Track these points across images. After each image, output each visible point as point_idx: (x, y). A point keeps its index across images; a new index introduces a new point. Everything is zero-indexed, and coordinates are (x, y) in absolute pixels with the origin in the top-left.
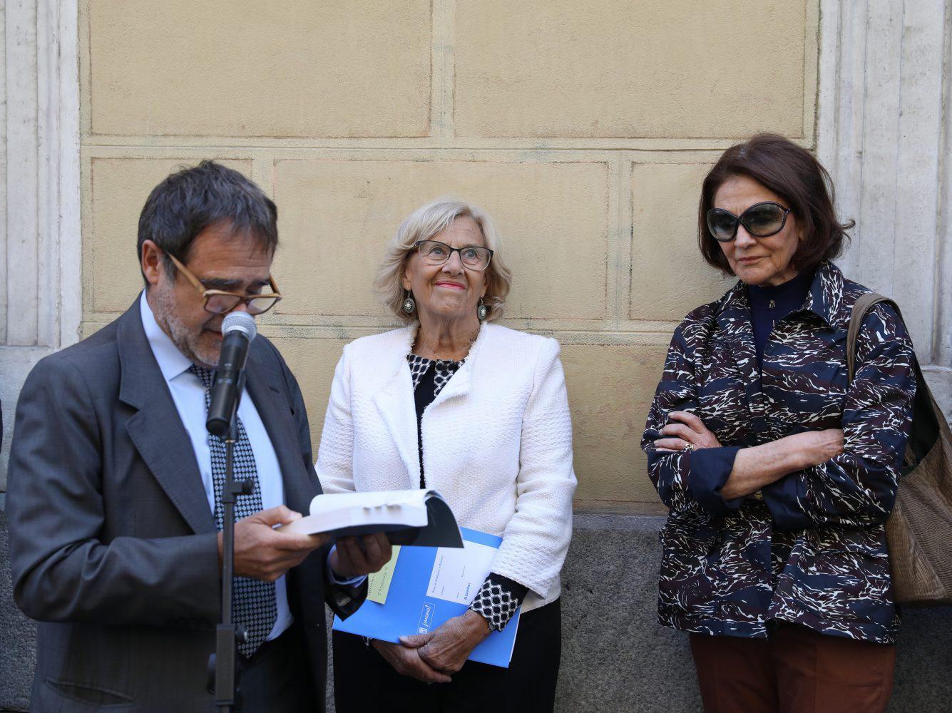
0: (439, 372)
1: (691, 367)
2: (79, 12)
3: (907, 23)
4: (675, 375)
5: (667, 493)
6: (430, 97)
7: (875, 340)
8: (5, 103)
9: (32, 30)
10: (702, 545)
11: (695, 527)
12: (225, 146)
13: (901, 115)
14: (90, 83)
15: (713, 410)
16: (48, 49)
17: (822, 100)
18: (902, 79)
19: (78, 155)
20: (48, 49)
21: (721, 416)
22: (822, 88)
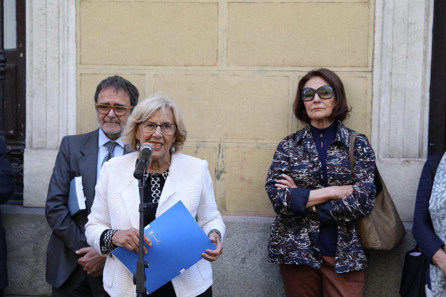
0: (153, 179)
1: (288, 159)
2: (76, 15)
3: (410, 21)
4: (280, 163)
5: (277, 210)
6: (217, 50)
7: (363, 151)
8: (46, 51)
9: (57, 22)
10: (290, 230)
11: (286, 223)
12: (134, 69)
13: (407, 58)
14: (80, 44)
15: (299, 176)
16: (64, 30)
17: (375, 52)
18: (408, 44)
19: (75, 72)
20: (64, 30)
21: (302, 179)
22: (375, 47)
